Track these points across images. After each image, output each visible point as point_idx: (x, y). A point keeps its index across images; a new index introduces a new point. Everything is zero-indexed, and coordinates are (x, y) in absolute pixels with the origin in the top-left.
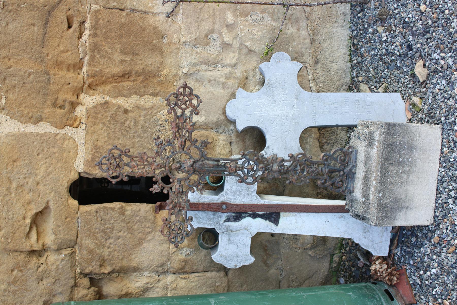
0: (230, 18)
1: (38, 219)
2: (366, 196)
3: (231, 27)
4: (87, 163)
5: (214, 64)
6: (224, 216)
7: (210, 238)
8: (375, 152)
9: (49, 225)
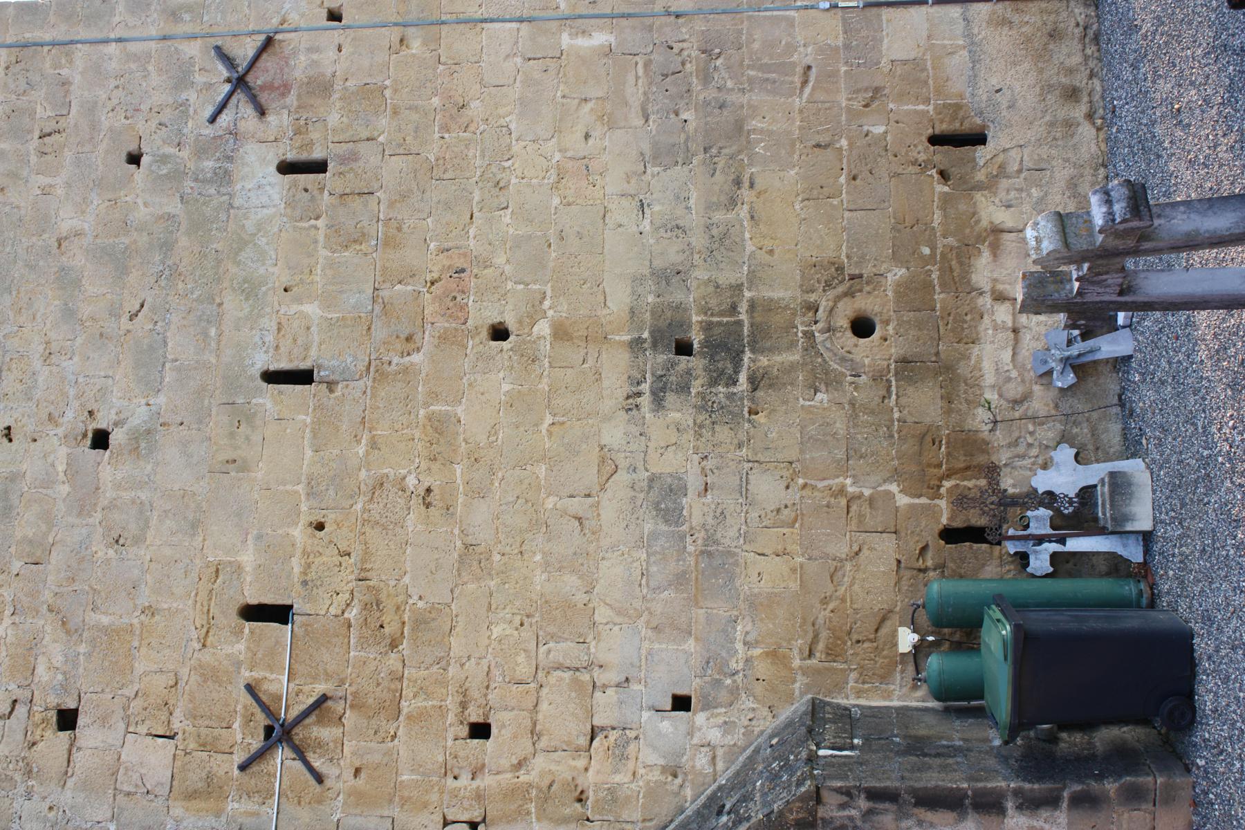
0: (1031, 428)
1: (924, 550)
2: (1104, 514)
3: (1031, 433)
4: (948, 519)
5: (1023, 457)
6: (1031, 543)
7: (1023, 558)
8: (1106, 489)
9: (929, 554)
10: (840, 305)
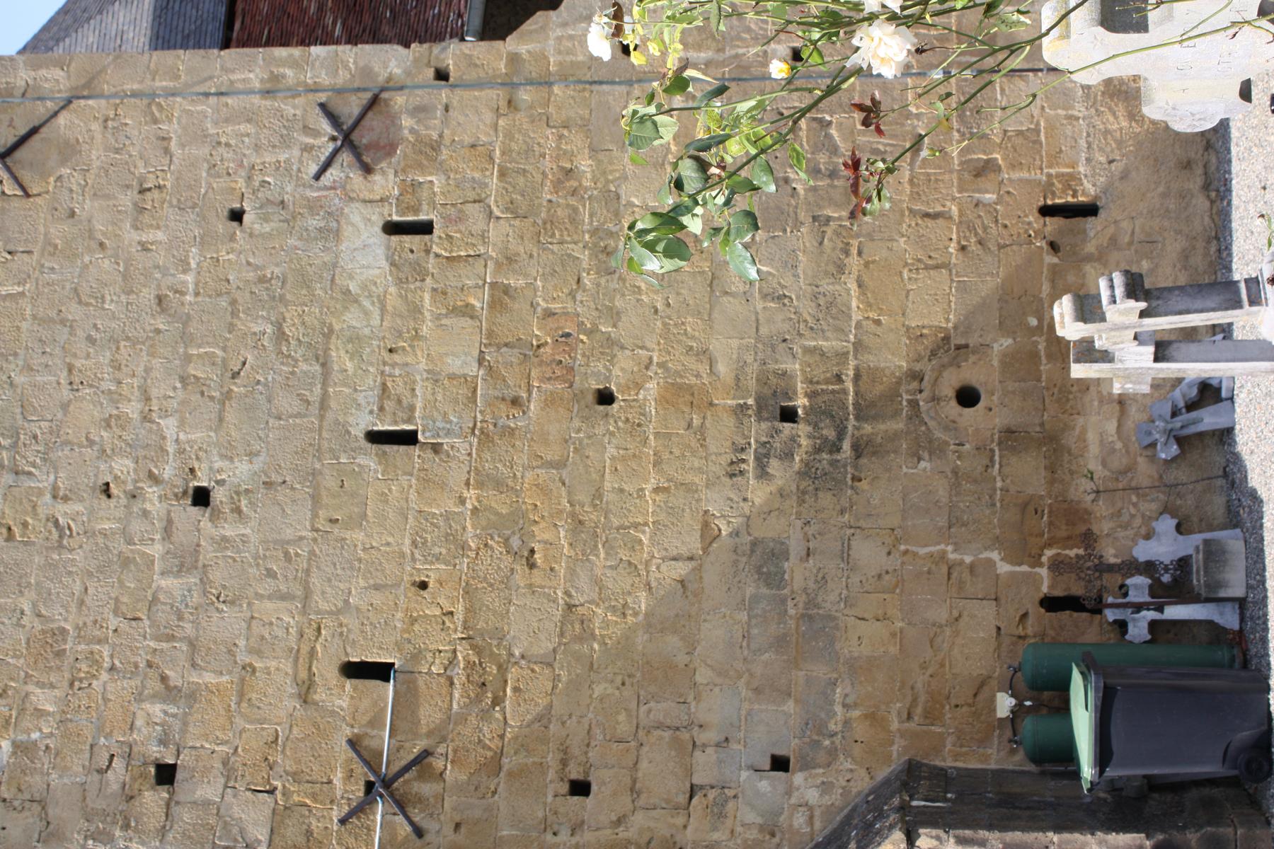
0: (1134, 499)
1: (1025, 616)
2: (1198, 581)
7: (1122, 626)
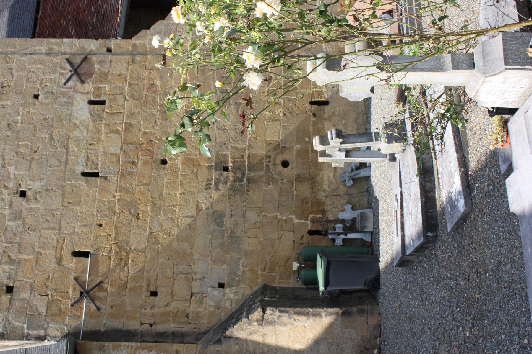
0: (338, 198)
1: (302, 237)
7: (334, 240)
9: (304, 238)
10: (278, 156)
